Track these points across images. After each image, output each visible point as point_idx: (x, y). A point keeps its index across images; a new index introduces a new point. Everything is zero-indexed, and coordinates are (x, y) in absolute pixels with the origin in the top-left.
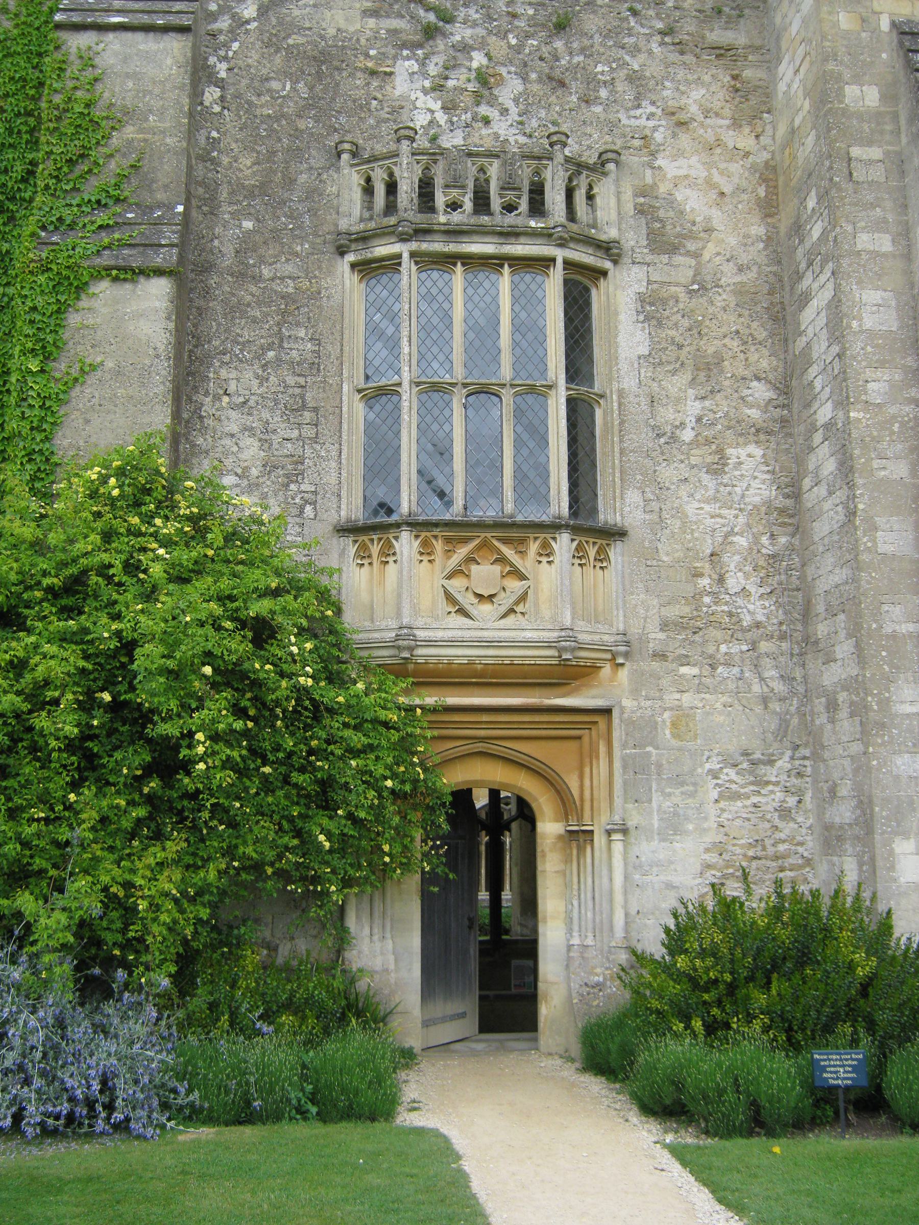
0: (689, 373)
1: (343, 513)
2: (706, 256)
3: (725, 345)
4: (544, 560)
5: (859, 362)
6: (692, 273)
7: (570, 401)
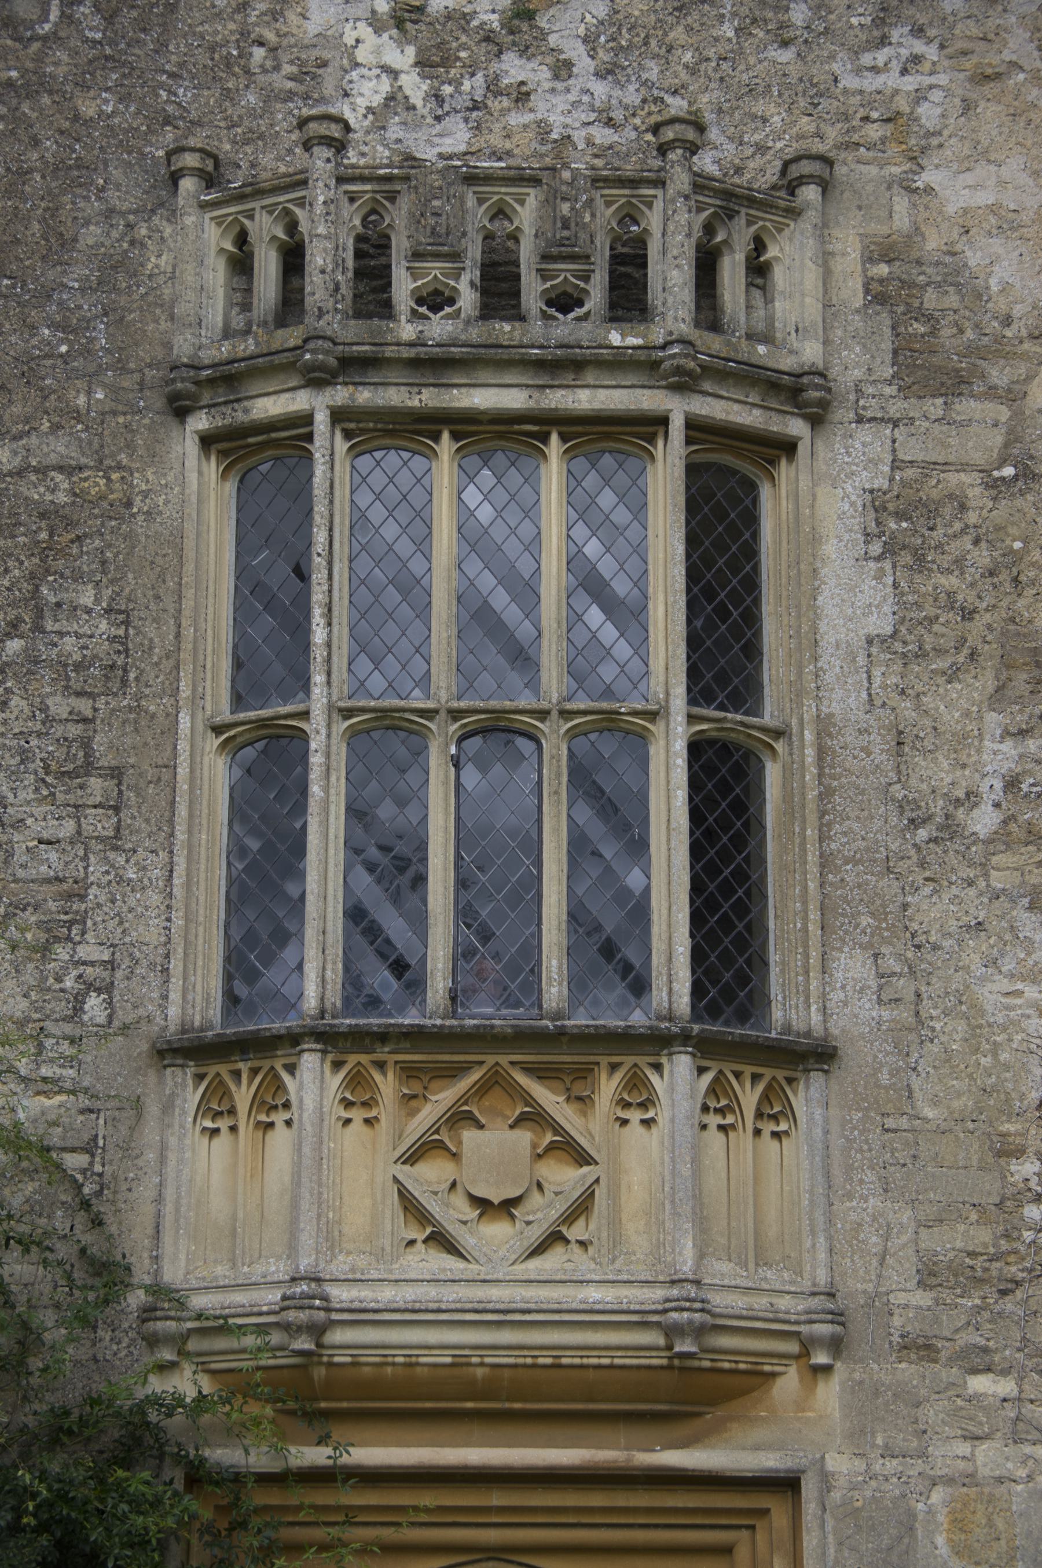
0: (990, 674)
1: (173, 1011)
4: (635, 1116)
6: (999, 440)
7: (695, 748)
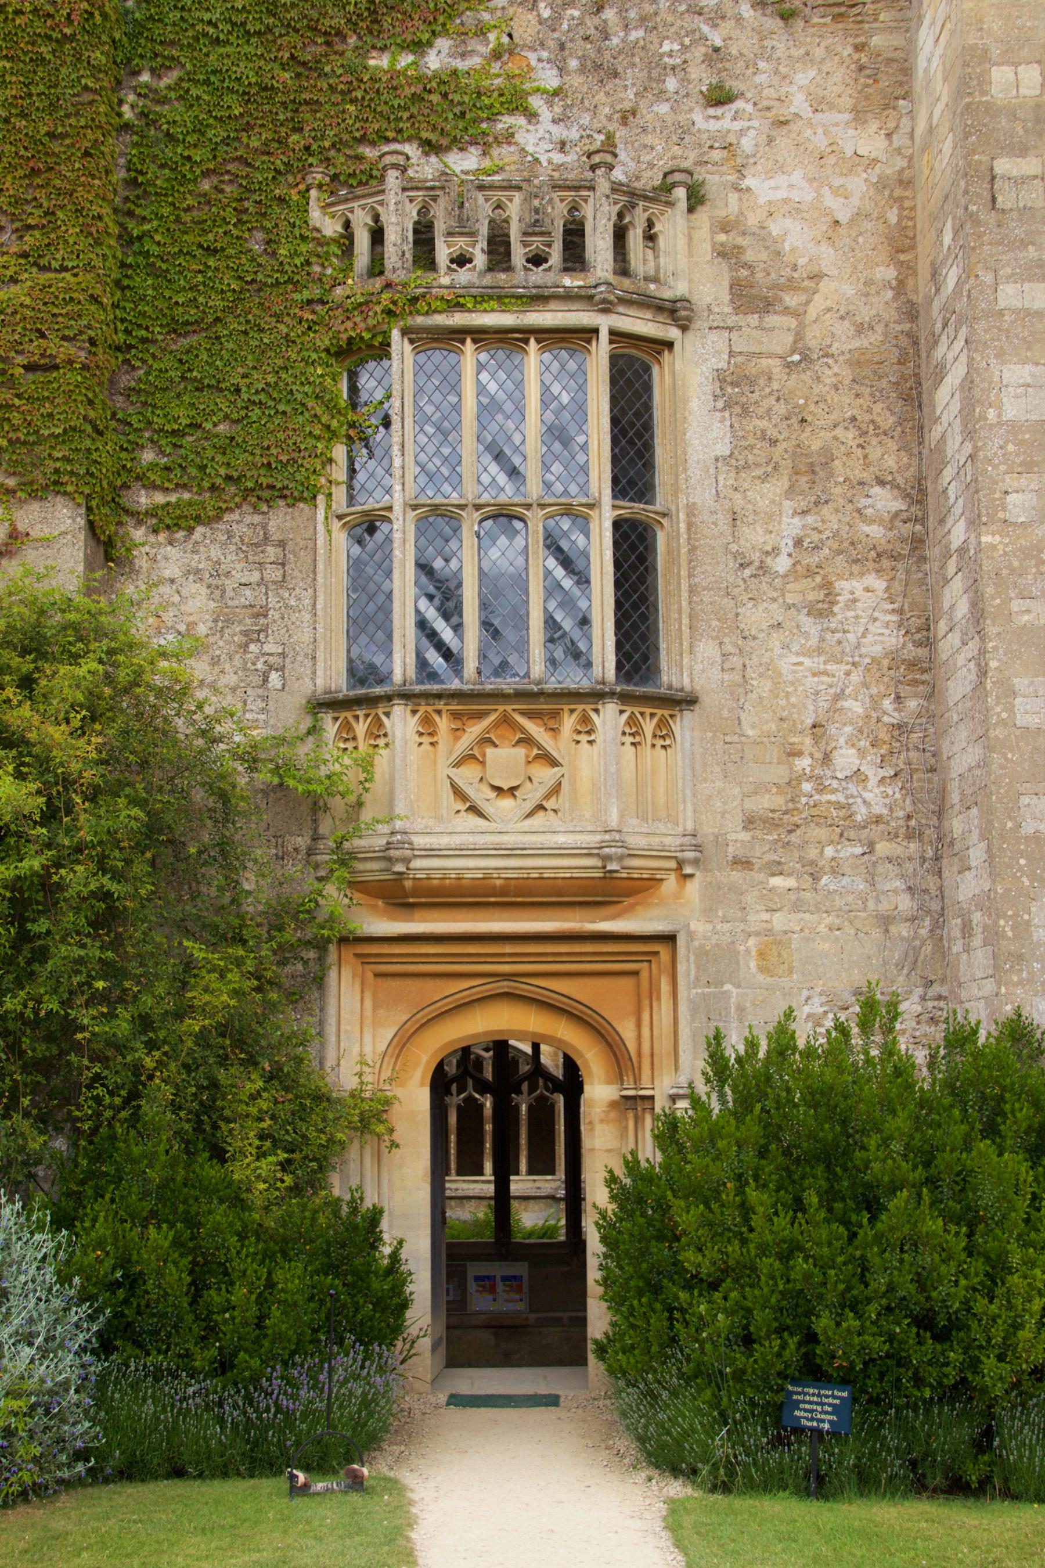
0: (786, 478)
2: (812, 312)
3: (836, 438)
4: (584, 738)
5: (995, 467)
6: (791, 339)
